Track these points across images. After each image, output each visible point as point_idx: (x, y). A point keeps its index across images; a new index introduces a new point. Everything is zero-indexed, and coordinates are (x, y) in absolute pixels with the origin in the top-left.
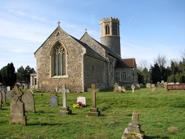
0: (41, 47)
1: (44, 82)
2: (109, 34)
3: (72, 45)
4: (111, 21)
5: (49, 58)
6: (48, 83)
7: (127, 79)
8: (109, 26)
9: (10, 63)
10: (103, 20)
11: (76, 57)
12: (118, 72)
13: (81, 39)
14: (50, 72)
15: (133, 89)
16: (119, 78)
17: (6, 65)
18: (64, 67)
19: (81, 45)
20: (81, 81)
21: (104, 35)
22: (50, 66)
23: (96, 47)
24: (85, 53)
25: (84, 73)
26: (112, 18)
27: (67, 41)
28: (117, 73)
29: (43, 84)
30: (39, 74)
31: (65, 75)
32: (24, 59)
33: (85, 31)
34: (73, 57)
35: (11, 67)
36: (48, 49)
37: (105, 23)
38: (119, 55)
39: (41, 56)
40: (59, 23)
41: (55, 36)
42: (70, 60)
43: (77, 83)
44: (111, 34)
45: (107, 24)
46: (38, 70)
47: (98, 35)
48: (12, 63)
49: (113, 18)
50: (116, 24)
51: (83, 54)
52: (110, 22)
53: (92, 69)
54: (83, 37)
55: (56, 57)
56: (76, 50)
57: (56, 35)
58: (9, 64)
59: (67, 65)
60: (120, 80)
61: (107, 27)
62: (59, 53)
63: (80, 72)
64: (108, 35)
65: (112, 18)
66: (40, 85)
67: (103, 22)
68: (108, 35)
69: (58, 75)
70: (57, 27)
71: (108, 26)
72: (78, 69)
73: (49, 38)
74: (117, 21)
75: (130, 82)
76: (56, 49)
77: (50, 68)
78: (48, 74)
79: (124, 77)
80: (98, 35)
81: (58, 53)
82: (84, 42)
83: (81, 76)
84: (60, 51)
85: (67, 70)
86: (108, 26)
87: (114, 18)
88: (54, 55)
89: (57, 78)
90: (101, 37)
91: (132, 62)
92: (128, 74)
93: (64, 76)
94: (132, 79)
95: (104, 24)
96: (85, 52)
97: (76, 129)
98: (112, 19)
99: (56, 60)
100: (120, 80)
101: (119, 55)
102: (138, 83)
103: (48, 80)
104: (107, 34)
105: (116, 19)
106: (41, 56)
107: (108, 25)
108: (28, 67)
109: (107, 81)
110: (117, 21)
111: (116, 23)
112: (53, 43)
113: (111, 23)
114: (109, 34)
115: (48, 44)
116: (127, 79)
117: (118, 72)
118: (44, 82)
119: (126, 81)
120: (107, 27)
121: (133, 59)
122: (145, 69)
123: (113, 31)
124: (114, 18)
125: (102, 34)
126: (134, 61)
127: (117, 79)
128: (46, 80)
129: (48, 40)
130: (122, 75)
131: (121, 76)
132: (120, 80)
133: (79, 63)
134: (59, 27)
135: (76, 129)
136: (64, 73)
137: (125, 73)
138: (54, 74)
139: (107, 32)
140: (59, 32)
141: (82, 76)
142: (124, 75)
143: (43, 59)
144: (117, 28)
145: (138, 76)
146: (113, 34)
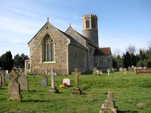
0: (33, 38)
1: (36, 67)
2: (89, 28)
3: (58, 36)
4: (90, 17)
5: (40, 47)
6: (39, 67)
7: (104, 64)
8: (89, 22)
9: (8, 51)
10: (84, 16)
11: (62, 46)
12: (96, 58)
13: (66, 32)
14: (41, 59)
15: (109, 72)
16: (97, 63)
17: (5, 53)
18: (52, 54)
19: (66, 37)
20: (66, 66)
21: (85, 29)
22: (41, 54)
23: (78, 38)
24: (69, 43)
25: (69, 59)
26: (91, 14)
27: (55, 33)
28: (96, 59)
29: (35, 68)
30: (32, 60)
31: (53, 61)
32: (20, 48)
33: (69, 26)
34: (60, 46)
35: (9, 54)
36: (39, 40)
37: (86, 18)
38: (97, 45)
39: (34, 45)
40: (48, 18)
41: (45, 29)
42: (57, 49)
43: (63, 68)
44: (90, 28)
45: (87, 20)
46: (31, 57)
47: (80, 28)
48: (10, 51)
49: (92, 15)
50: (94, 19)
51: (67, 44)
52: (90, 18)
53: (75, 56)
54: (68, 30)
55: (46, 46)
56: (62, 40)
57: (46, 29)
58: (7, 52)
59: (54, 53)
60: (98, 65)
61: (87, 22)
62: (48, 43)
63: (66, 59)
64: (88, 29)
65: (91, 14)
66: (33, 69)
67: (84, 18)
68: (88, 29)
69: (48, 61)
70: (47, 22)
71: (88, 22)
72: (64, 56)
73: (40, 31)
74: (96, 17)
75: (106, 66)
76: (46, 40)
77: (40, 56)
78: (39, 60)
79: (101, 63)
80: (80, 28)
81: (47, 43)
82: (68, 34)
83: (66, 62)
84: (49, 42)
85: (54, 57)
86: (88, 22)
87: (93, 15)
88: (44, 45)
89: (47, 64)
90: (82, 30)
91: (108, 50)
92: (104, 60)
93: (52, 62)
94: (108, 64)
95: (85, 19)
96: (70, 43)
97: (62, 105)
98: (91, 16)
99: (46, 48)
100: (98, 65)
101: (97, 45)
102: (113, 67)
103: (39, 65)
104: (87, 27)
105: (94, 15)
106: (34, 45)
107: (88, 20)
108: (23, 55)
109: (88, 66)
110: (96, 17)
111: (94, 19)
112: (43, 35)
113: (90, 18)
114: (89, 28)
115: (39, 36)
116: (104, 64)
117: (96, 58)
118: (36, 67)
119: (103, 66)
120: (87, 22)
121: (109, 48)
122: (119, 56)
123: (92, 25)
124: (93, 15)
125: (83, 28)
126: (109, 50)
127: (95, 64)
128: (38, 65)
129: (40, 32)
130: (99, 61)
131: (98, 61)
132: (98, 65)
133: (65, 51)
134: (48, 22)
135: (62, 105)
136: (52, 59)
137: (102, 59)
138: (44, 60)
139: (87, 26)
140: (48, 26)
141: (67, 62)
142: (101, 61)
143: (35, 48)
144: (95, 23)
145: (113, 62)
146: (92, 27)
